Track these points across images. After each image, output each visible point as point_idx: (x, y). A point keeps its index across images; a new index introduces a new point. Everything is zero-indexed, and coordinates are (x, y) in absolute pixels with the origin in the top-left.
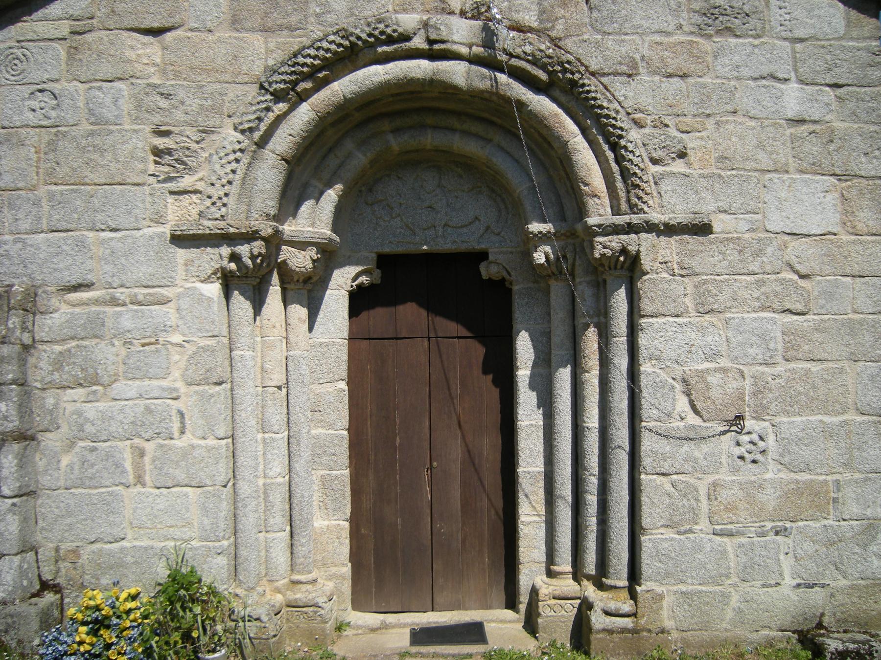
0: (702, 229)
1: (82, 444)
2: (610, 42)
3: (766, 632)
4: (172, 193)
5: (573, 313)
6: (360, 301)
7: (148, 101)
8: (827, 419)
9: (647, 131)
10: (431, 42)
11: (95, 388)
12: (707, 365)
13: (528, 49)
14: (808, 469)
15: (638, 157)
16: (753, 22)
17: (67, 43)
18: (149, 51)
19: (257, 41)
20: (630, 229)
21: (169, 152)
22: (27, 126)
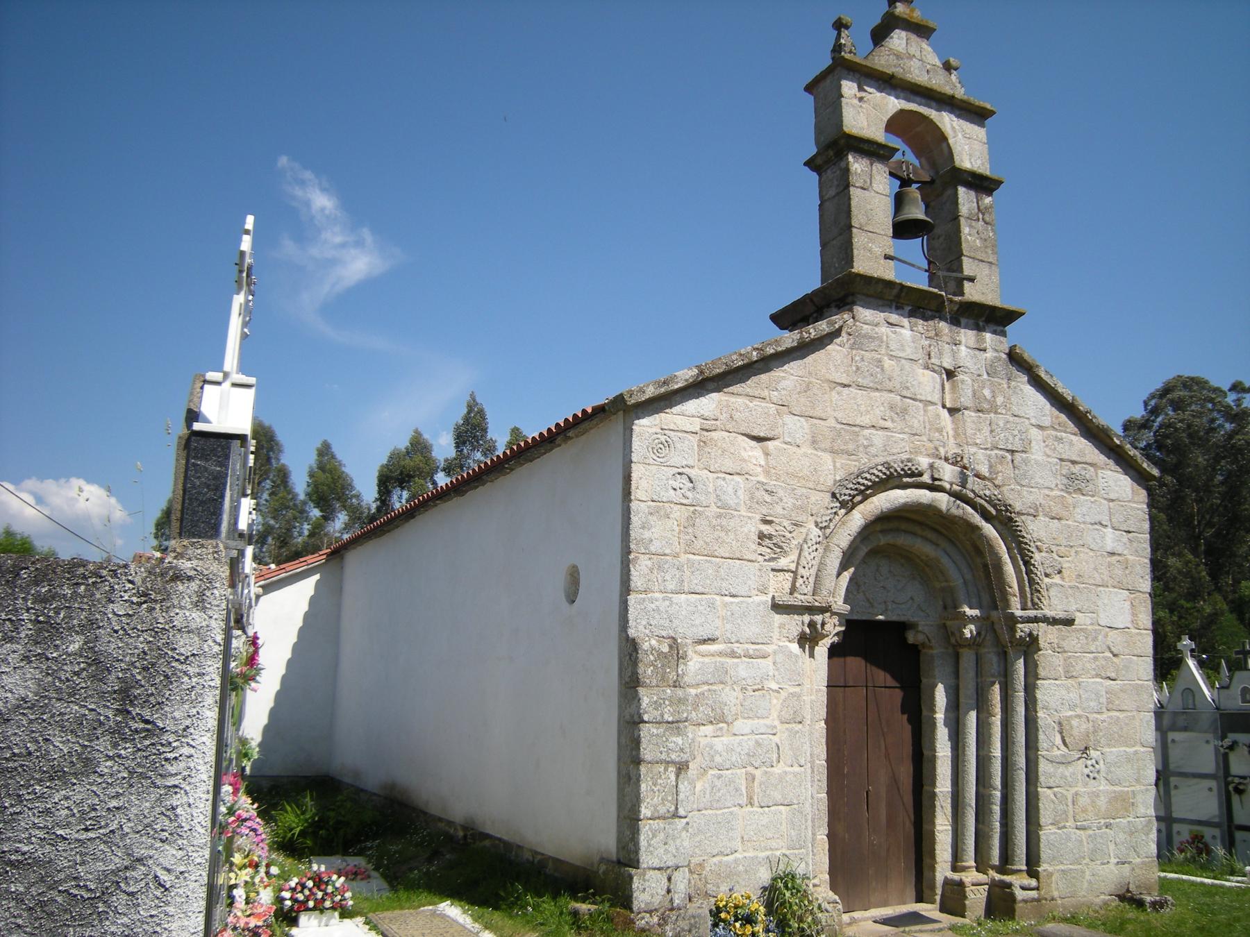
0: (1069, 622)
1: (711, 772)
2: (1025, 491)
3: (1102, 897)
4: (773, 570)
5: (978, 673)
6: (834, 651)
7: (758, 494)
8: (1128, 749)
9: (1043, 554)
10: (934, 479)
11: (721, 725)
12: (1070, 713)
13: (987, 493)
14: (1119, 784)
15: (1039, 571)
16: (1091, 486)
17: (697, 437)
18: (753, 452)
19: (827, 458)
20: (1035, 620)
21: (770, 537)
22: (671, 502)
